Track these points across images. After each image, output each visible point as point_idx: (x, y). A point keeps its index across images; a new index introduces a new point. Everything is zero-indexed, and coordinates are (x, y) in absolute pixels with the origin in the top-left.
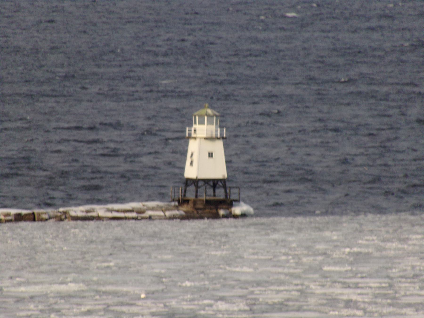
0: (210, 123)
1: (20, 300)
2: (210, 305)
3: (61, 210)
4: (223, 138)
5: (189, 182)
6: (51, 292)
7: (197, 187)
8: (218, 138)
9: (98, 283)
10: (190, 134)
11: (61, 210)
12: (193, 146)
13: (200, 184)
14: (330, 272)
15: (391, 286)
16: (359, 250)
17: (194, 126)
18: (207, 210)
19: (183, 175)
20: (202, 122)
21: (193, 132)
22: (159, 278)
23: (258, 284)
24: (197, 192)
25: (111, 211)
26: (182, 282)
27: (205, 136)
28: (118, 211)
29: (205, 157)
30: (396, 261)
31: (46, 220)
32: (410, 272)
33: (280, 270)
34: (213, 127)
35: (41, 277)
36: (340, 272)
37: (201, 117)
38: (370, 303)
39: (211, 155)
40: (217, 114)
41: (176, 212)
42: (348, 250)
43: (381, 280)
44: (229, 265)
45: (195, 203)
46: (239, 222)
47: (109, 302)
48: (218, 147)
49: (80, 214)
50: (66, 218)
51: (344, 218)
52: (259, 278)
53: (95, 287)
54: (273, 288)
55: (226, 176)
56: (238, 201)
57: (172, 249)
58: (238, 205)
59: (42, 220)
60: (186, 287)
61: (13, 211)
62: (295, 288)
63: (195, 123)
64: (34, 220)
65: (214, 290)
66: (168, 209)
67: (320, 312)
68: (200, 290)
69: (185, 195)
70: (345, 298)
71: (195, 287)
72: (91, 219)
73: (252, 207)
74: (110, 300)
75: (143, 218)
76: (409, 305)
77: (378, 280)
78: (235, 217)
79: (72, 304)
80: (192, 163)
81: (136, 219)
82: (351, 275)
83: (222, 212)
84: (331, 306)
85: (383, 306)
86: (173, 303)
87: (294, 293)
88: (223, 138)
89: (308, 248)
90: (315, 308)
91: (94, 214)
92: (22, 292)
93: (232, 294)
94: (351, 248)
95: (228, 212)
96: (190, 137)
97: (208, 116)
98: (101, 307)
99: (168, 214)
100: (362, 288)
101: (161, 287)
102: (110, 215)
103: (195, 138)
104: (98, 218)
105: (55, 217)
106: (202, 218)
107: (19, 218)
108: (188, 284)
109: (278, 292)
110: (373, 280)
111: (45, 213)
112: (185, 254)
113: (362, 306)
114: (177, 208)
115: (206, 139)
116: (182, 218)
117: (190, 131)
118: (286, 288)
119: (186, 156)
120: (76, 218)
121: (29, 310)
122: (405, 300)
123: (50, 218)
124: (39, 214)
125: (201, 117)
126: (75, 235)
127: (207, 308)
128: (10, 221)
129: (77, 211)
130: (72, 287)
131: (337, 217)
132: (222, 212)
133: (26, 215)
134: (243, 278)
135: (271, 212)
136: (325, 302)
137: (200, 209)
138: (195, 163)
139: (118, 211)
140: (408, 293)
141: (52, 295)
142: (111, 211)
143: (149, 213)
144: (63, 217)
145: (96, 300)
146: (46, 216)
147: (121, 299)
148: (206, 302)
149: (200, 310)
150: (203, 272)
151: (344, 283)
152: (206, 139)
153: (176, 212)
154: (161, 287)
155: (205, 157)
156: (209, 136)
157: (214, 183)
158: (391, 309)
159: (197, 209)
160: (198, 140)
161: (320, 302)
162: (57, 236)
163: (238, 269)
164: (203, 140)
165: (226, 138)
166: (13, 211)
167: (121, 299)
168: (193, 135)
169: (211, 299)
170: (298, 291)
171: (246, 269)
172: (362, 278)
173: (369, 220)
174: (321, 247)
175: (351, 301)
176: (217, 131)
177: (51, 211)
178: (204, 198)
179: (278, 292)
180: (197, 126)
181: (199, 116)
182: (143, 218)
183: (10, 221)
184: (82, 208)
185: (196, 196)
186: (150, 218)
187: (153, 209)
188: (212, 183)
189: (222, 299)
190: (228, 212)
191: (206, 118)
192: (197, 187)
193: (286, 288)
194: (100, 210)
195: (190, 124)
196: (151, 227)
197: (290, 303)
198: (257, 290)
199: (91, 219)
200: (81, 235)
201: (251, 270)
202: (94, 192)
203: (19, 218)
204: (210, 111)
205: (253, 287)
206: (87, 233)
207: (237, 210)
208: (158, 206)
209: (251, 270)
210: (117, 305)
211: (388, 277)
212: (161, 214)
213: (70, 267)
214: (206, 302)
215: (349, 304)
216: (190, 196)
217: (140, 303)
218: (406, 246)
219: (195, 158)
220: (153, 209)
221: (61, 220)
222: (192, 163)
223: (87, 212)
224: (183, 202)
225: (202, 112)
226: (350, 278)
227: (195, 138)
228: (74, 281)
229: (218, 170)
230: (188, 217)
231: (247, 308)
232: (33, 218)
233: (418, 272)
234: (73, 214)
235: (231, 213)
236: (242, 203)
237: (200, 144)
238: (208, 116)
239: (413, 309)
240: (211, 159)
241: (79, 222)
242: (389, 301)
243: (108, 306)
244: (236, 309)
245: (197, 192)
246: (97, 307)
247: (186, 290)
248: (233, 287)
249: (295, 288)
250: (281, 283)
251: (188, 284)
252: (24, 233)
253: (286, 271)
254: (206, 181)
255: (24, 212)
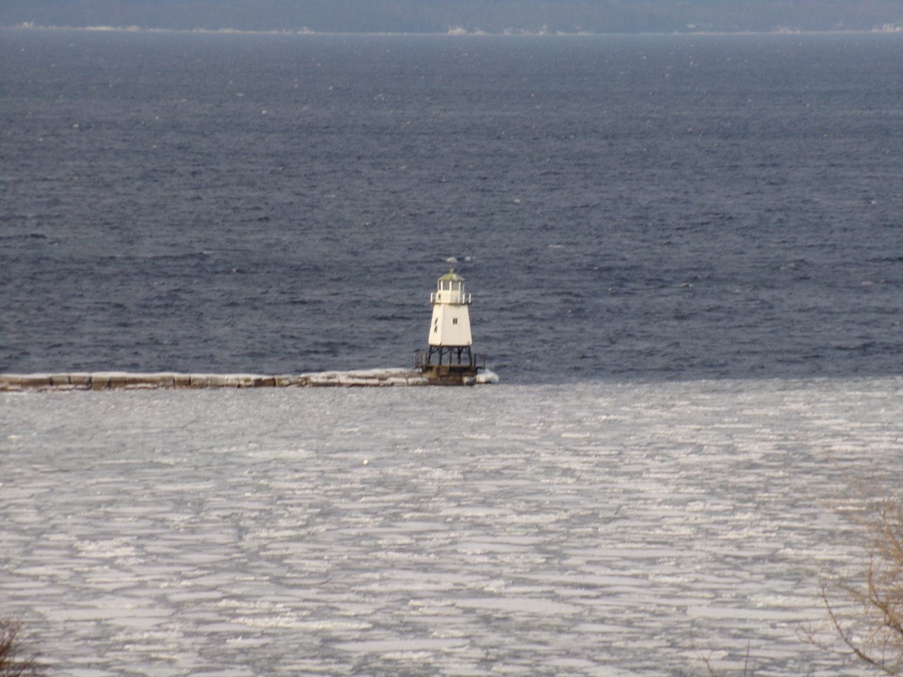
3: (303, 375)
5: (433, 349)
7: (441, 354)
10: (434, 300)
13: (444, 350)
17: (439, 292)
18: (451, 378)
20: (446, 288)
24: (441, 358)
25: (353, 377)
27: (449, 301)
28: (359, 377)
29: (449, 322)
31: (287, 386)
34: (458, 293)
36: (576, 439)
39: (455, 321)
40: (463, 279)
41: (419, 379)
42: (604, 417)
43: (611, 448)
45: (438, 369)
48: (463, 314)
49: (321, 380)
56: (483, 368)
58: (483, 373)
59: (282, 386)
61: (254, 377)
64: (274, 385)
66: (410, 376)
70: (565, 466)
72: (333, 385)
75: (385, 385)
76: (626, 474)
77: (609, 448)
79: (692, 444)
80: (436, 329)
82: (585, 443)
83: (466, 380)
88: (467, 303)
91: (335, 380)
94: (608, 415)
95: (472, 379)
96: (434, 303)
99: (411, 380)
102: (351, 381)
103: (440, 304)
104: (340, 385)
105: (297, 383)
107: (259, 383)
110: (605, 448)
111: (286, 379)
114: (420, 374)
115: (451, 304)
116: (425, 384)
117: (434, 296)
119: (430, 323)
120: (317, 385)
121: (244, 476)
123: (290, 384)
124: (280, 380)
127: (420, 476)
128: (251, 386)
131: (571, 385)
132: (466, 380)
133: (266, 381)
137: (445, 376)
138: (439, 329)
139: (359, 377)
142: (353, 377)
143: (391, 380)
144: (304, 383)
151: (574, 451)
153: (419, 379)
155: (449, 322)
156: (454, 301)
157: (460, 349)
159: (441, 376)
163: (475, 436)
164: (447, 306)
166: (254, 377)
168: (437, 301)
171: (484, 436)
172: (596, 445)
175: (570, 469)
176: (461, 296)
178: (448, 365)
180: (441, 292)
182: (385, 385)
183: (251, 386)
184: (323, 374)
185: (440, 363)
186: (392, 384)
187: (395, 376)
188: (456, 350)
190: (472, 379)
192: (441, 354)
194: (342, 377)
195: (435, 288)
196: (395, 394)
197: (507, 471)
199: (333, 385)
200: (357, 399)
201: (488, 437)
203: (259, 383)
204: (454, 276)
207: (481, 377)
208: (401, 373)
209: (488, 437)
210: (334, 472)
212: (404, 380)
215: (567, 472)
216: (435, 362)
220: (395, 376)
222: (436, 329)
223: (329, 378)
224: (427, 368)
225: (447, 277)
226: (585, 445)
227: (440, 304)
230: (431, 383)
231: (460, 476)
232: (273, 383)
234: (314, 380)
235: (475, 380)
236: (487, 371)
237: (444, 311)
238: (453, 282)
240: (455, 325)
241: (322, 389)
242: (607, 469)
245: (441, 358)
252: (300, 397)
254: (451, 348)
255: (264, 377)
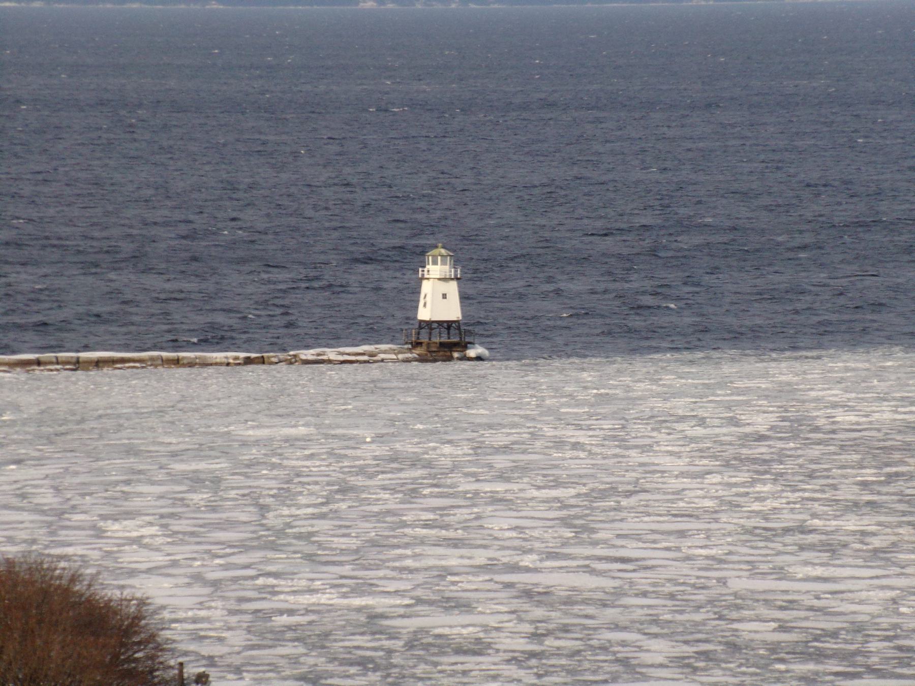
0: (444, 263)
1: (244, 444)
2: (434, 449)
3: (292, 353)
6: (280, 435)
8: (452, 279)
9: (330, 426)
10: (423, 275)
11: (292, 353)
14: (567, 413)
15: (624, 427)
16: (607, 391)
18: (441, 353)
19: (416, 318)
20: (435, 263)
21: (426, 273)
22: (392, 421)
23: (490, 426)
25: (342, 354)
26: (414, 425)
28: (349, 354)
30: (639, 402)
32: (648, 413)
33: (516, 412)
34: (447, 268)
35: (277, 421)
36: (576, 413)
38: (597, 445)
39: (444, 296)
41: (409, 355)
42: (595, 391)
43: (613, 422)
44: (468, 407)
46: (307, 370)
47: (335, 446)
48: (453, 288)
49: (310, 358)
50: (296, 361)
51: (897, 349)
52: (495, 420)
53: (325, 431)
54: (504, 430)
57: (419, 392)
60: (419, 429)
61: (243, 355)
62: (527, 430)
64: (263, 363)
65: (446, 433)
67: (544, 454)
68: (431, 433)
69: (418, 338)
70: (573, 440)
71: (426, 430)
74: (336, 444)
76: (636, 447)
80: (425, 305)
83: (456, 355)
84: (557, 449)
85: (610, 447)
86: (398, 446)
87: (524, 435)
88: (458, 279)
89: (556, 390)
90: (540, 451)
92: (249, 436)
93: (460, 437)
96: (423, 278)
97: (442, 256)
98: (324, 450)
99: (401, 356)
100: (594, 429)
101: (392, 430)
102: (341, 358)
104: (330, 361)
105: (285, 361)
106: (435, 361)
108: (421, 427)
109: (509, 434)
112: (429, 397)
113: (589, 448)
114: (410, 350)
115: (440, 279)
118: (518, 430)
122: (633, 442)
123: (280, 362)
124: (269, 357)
126: (330, 376)
128: (239, 364)
129: (308, 354)
130: (302, 430)
132: (456, 355)
134: (478, 421)
136: (551, 444)
138: (428, 305)
139: (349, 354)
140: (639, 435)
141: (279, 438)
142: (342, 354)
143: (382, 356)
145: (321, 444)
146: (275, 360)
147: (346, 443)
148: (431, 445)
149: (424, 454)
150: (437, 415)
152: (440, 279)
153: (409, 355)
154: (392, 430)
155: (439, 297)
157: (448, 325)
158: (617, 451)
161: (546, 444)
162: (313, 378)
166: (243, 355)
167: (346, 443)
168: (426, 276)
169: (437, 442)
170: (529, 433)
173: (620, 362)
174: (569, 389)
175: (579, 443)
177: (282, 356)
178: (437, 340)
179: (509, 434)
180: (430, 267)
181: (433, 256)
183: (239, 364)
184: (312, 351)
186: (382, 361)
188: (445, 325)
189: (449, 442)
193: (518, 430)
194: (331, 354)
198: (487, 433)
202: (214, 338)
203: (248, 361)
204: (443, 251)
205: (485, 430)
206: (344, 376)
207: (472, 353)
211: (623, 418)
213: (307, 410)
214: (431, 445)
215: (576, 446)
216: (424, 339)
217: (364, 447)
218: (654, 387)
219: (428, 299)
220: (385, 352)
221: (291, 363)
222: (425, 305)
223: (318, 355)
224: (418, 344)
225: (435, 252)
226: (584, 420)
228: (306, 425)
229: (452, 311)
231: (471, 452)
232: (262, 361)
233: (656, 413)
234: (303, 357)
235: (465, 356)
238: (442, 256)
239: (639, 450)
243: (333, 449)
244: (460, 452)
246: (322, 451)
247: (418, 433)
248: (465, 430)
249: (527, 430)
250: (514, 425)
251: (421, 427)
252: (278, 375)
253: (522, 413)
254: (440, 323)
255: (253, 355)
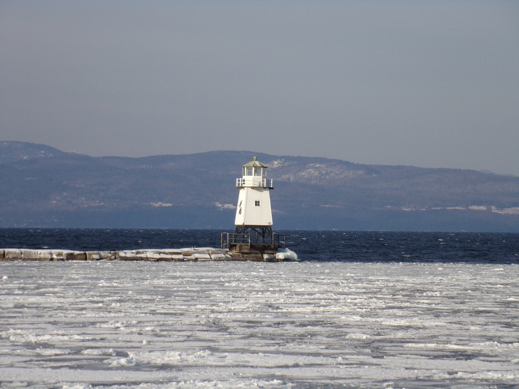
4: (270, 188)
8: (265, 188)
12: (242, 194)
17: (244, 177)
20: (250, 174)
27: (251, 186)
37: (249, 168)
39: (257, 203)
48: (265, 196)
55: (272, 224)
61: (65, 252)
63: (244, 175)
73: (295, 251)
75: (189, 260)
78: (278, 260)
81: (183, 260)
88: (270, 188)
97: (256, 167)
99: (213, 256)
103: (243, 188)
115: (253, 188)
116: (228, 259)
125: (249, 168)
132: (266, 256)
135: (199, 269)
137: (247, 253)
138: (243, 212)
152: (253, 188)
156: (257, 185)
160: (246, 188)
165: (272, 188)
180: (245, 177)
181: (247, 167)
182: (189, 260)
186: (196, 260)
191: (253, 168)
204: (257, 163)
219: (243, 206)
222: (240, 212)
225: (251, 164)
